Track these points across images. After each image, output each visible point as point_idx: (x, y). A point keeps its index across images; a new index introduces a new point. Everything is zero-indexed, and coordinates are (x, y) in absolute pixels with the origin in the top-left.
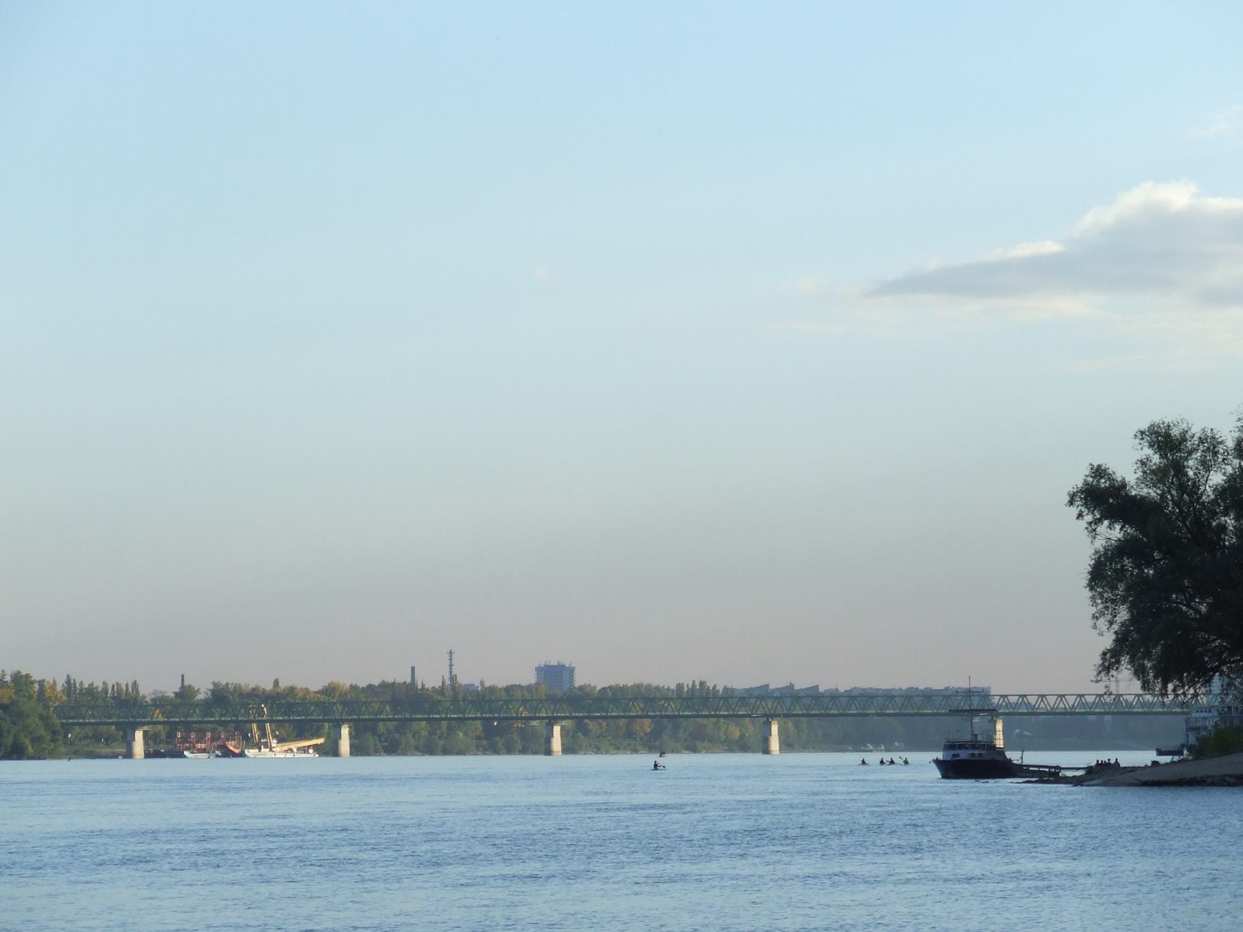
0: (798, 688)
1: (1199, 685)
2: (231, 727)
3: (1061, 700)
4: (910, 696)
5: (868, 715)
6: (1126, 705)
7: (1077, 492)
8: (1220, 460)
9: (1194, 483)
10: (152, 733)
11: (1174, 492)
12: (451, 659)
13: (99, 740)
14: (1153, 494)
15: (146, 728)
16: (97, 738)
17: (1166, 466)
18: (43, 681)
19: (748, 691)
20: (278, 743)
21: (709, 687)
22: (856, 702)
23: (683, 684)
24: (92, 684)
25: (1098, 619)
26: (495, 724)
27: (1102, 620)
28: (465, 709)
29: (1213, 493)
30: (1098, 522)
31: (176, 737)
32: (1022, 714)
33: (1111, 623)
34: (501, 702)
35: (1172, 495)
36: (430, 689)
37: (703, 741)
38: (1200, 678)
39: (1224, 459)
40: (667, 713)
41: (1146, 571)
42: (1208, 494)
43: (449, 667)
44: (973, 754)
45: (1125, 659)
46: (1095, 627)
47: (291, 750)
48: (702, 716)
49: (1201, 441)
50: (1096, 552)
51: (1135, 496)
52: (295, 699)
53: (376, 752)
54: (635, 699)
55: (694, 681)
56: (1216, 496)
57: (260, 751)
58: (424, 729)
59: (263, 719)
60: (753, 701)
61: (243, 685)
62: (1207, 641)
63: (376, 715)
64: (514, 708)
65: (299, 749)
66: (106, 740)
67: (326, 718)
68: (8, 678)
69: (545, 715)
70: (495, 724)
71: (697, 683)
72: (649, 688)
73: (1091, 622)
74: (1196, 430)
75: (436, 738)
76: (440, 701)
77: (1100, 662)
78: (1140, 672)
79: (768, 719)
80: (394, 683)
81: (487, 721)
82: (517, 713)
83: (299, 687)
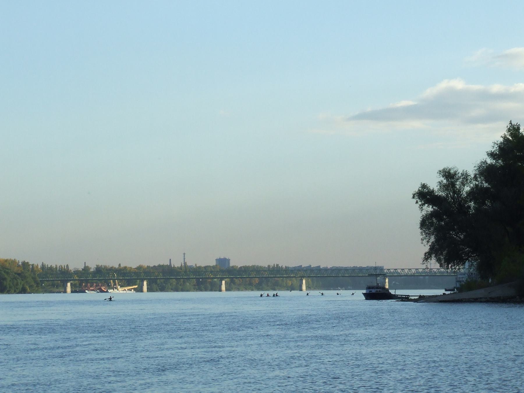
2: (103, 282)
4: (354, 269)
7: (416, 193)
11: (451, 194)
12: (184, 256)
15: (71, 282)
16: (53, 285)
18: (34, 264)
20: (120, 287)
25: (423, 240)
26: (201, 280)
30: (424, 204)
33: (428, 242)
35: (450, 195)
42: (464, 194)
44: (377, 291)
45: (433, 256)
46: (422, 243)
48: (277, 277)
49: (462, 174)
50: (423, 216)
51: (437, 195)
54: (252, 271)
55: (274, 264)
57: (114, 290)
58: (174, 282)
60: (296, 271)
61: (107, 266)
65: (128, 289)
68: (20, 264)
70: (201, 280)
72: (258, 267)
73: (421, 241)
76: (180, 272)
80: (163, 265)
82: (209, 276)
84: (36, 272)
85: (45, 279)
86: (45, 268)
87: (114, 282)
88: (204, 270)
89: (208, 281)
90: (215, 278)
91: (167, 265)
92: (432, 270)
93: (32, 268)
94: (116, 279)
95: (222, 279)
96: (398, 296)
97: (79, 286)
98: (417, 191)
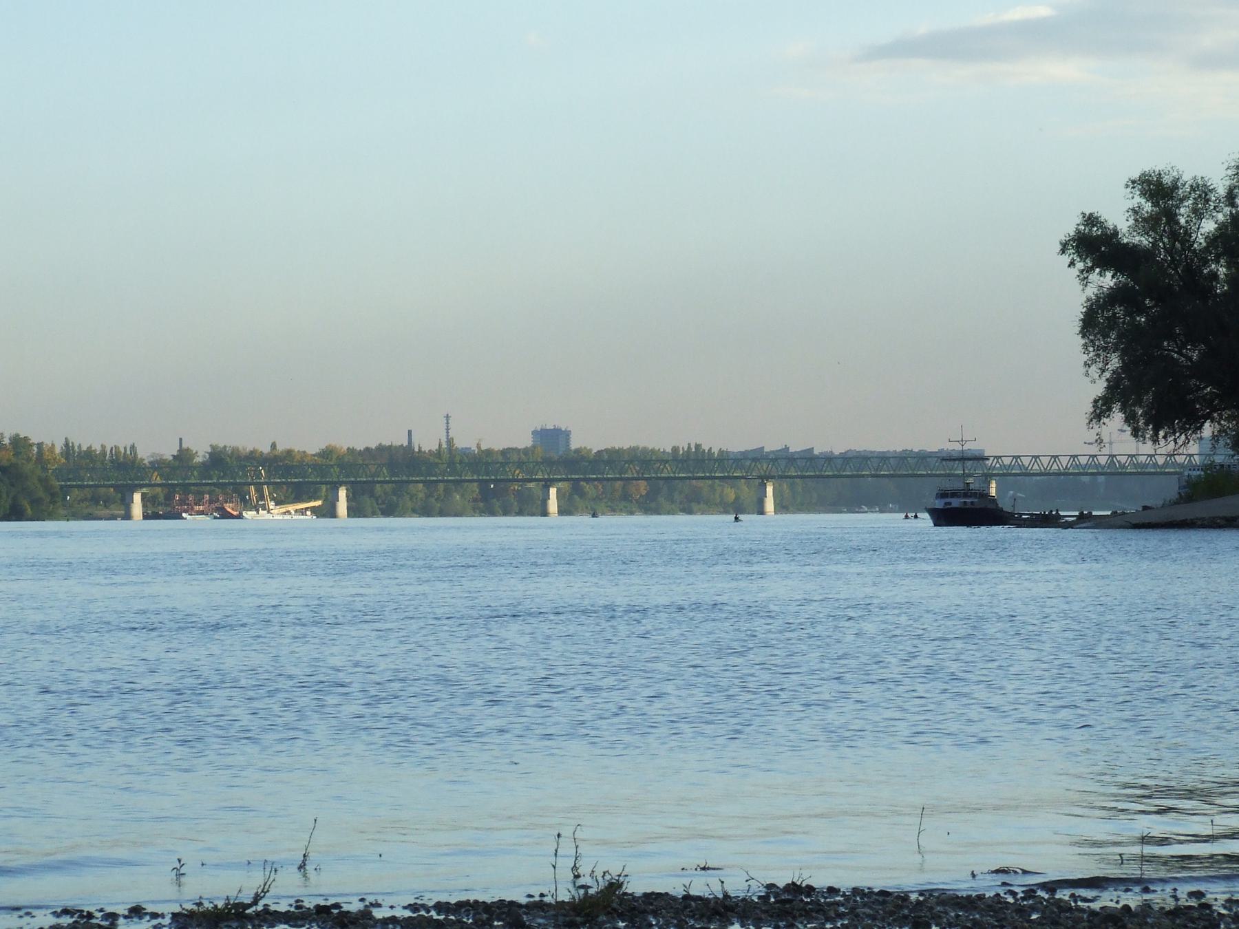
0: (793, 451)
1: (1190, 432)
2: (229, 489)
3: (1055, 460)
4: (903, 458)
5: (863, 476)
6: (1119, 466)
7: (1069, 240)
10: (150, 495)
11: (1166, 240)
12: (448, 423)
13: (97, 503)
15: (144, 490)
16: (95, 500)
17: (1157, 214)
19: (742, 453)
21: (704, 450)
23: (678, 447)
24: (91, 447)
25: (1089, 367)
26: (492, 486)
27: (1093, 368)
28: (462, 472)
29: (1205, 241)
30: (1089, 270)
31: (174, 499)
33: (1103, 371)
34: (499, 465)
35: (1164, 243)
36: (427, 452)
37: (699, 503)
38: (1191, 425)
39: (1215, 208)
40: (663, 475)
41: (1138, 319)
42: (1200, 241)
44: (965, 502)
45: (1116, 407)
46: (1087, 374)
48: (699, 478)
49: (1193, 189)
50: (1088, 300)
51: (1128, 244)
52: (293, 462)
53: (373, 514)
54: (631, 462)
55: (689, 444)
56: (1208, 243)
57: (258, 512)
58: (421, 491)
59: (261, 481)
60: (748, 463)
61: (241, 448)
62: (1199, 389)
64: (510, 471)
65: (296, 511)
66: (104, 502)
67: (324, 480)
68: (6, 441)
69: (541, 477)
70: (492, 486)
71: (693, 447)
72: (645, 450)
73: (1083, 370)
75: (433, 500)
76: (437, 464)
77: (1092, 410)
78: (1130, 419)
79: (763, 481)
80: (391, 446)
81: (483, 484)
82: (513, 475)
83: (296, 450)
84: (49, 463)
85: (75, 483)
86: (74, 453)
87: (260, 491)
88: (500, 459)
89: (512, 488)
90: (530, 481)
91: (402, 445)
92: (1114, 459)
93: (38, 452)
95: (549, 483)
96: (1024, 517)
97: (163, 501)
98: (1072, 232)
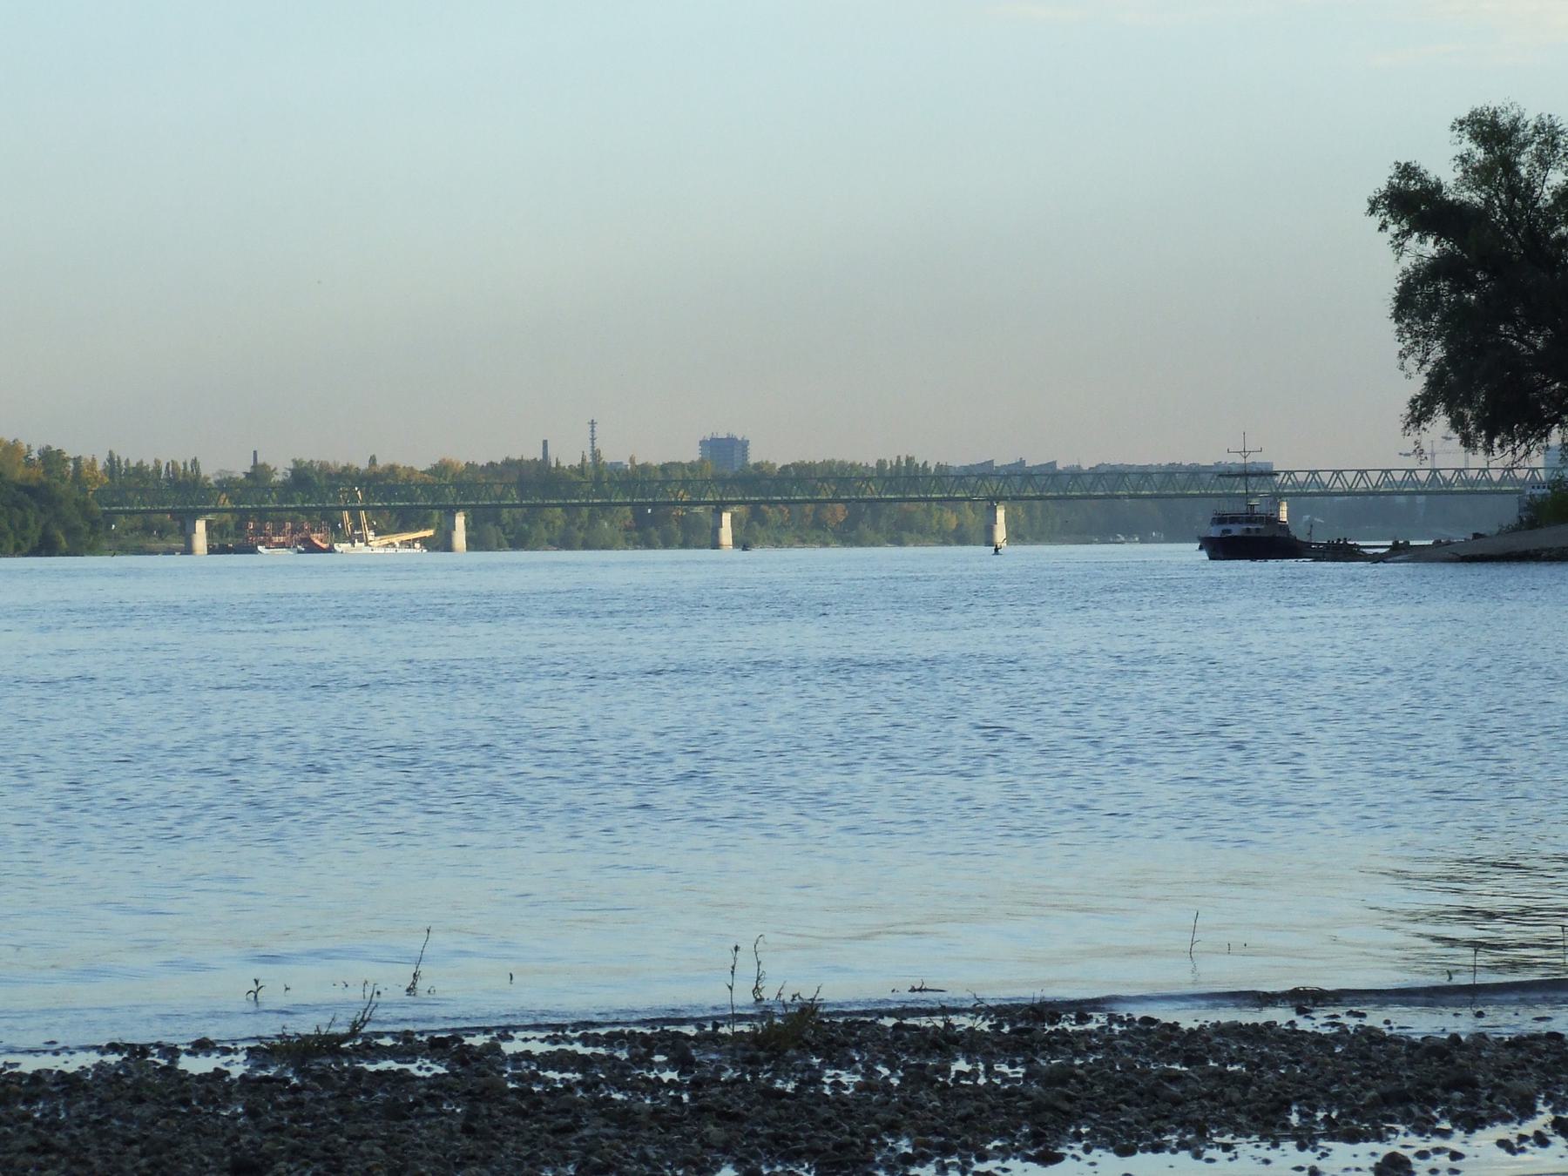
4: (1169, 473)
5: (1118, 497)
8: (1561, 155)
9: (1528, 184)
11: (1503, 197)
12: (593, 431)
14: (1477, 200)
15: (209, 517)
16: (147, 529)
17: (1492, 163)
22: (1104, 482)
23: (885, 461)
24: (142, 462)
25: (1406, 357)
26: (649, 511)
27: (1411, 359)
30: (1406, 234)
32: (1310, 494)
33: (1423, 362)
35: (1500, 200)
40: (865, 496)
42: (1546, 196)
43: (590, 441)
45: (1440, 408)
47: (392, 545)
49: (1537, 130)
51: (1454, 200)
53: (499, 547)
54: (824, 479)
55: (899, 457)
56: (1555, 200)
60: (973, 480)
61: (331, 463)
63: (499, 500)
66: (160, 532)
67: (436, 504)
68: (35, 455)
70: (649, 511)
71: (903, 460)
72: (842, 465)
73: (1398, 362)
74: (1531, 118)
77: (1409, 411)
78: (1457, 423)
79: (992, 504)
80: (521, 461)
81: (638, 508)
82: (676, 496)
83: (401, 466)
94: (362, 508)
